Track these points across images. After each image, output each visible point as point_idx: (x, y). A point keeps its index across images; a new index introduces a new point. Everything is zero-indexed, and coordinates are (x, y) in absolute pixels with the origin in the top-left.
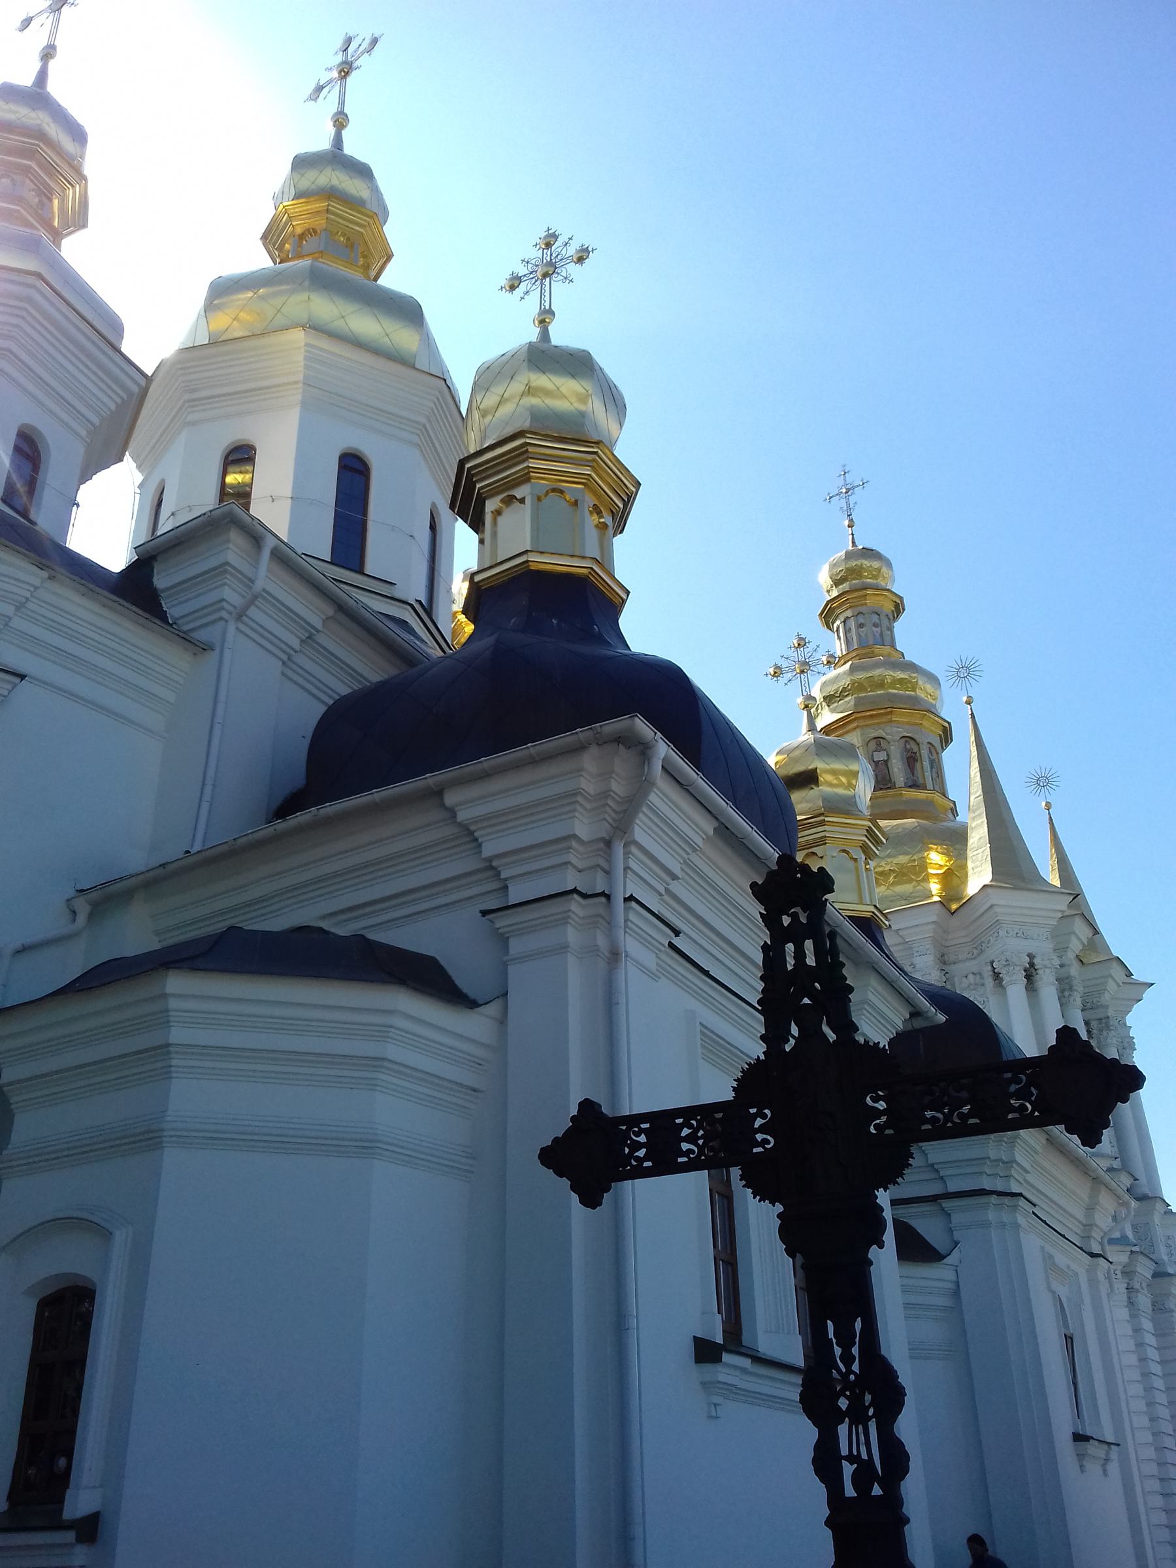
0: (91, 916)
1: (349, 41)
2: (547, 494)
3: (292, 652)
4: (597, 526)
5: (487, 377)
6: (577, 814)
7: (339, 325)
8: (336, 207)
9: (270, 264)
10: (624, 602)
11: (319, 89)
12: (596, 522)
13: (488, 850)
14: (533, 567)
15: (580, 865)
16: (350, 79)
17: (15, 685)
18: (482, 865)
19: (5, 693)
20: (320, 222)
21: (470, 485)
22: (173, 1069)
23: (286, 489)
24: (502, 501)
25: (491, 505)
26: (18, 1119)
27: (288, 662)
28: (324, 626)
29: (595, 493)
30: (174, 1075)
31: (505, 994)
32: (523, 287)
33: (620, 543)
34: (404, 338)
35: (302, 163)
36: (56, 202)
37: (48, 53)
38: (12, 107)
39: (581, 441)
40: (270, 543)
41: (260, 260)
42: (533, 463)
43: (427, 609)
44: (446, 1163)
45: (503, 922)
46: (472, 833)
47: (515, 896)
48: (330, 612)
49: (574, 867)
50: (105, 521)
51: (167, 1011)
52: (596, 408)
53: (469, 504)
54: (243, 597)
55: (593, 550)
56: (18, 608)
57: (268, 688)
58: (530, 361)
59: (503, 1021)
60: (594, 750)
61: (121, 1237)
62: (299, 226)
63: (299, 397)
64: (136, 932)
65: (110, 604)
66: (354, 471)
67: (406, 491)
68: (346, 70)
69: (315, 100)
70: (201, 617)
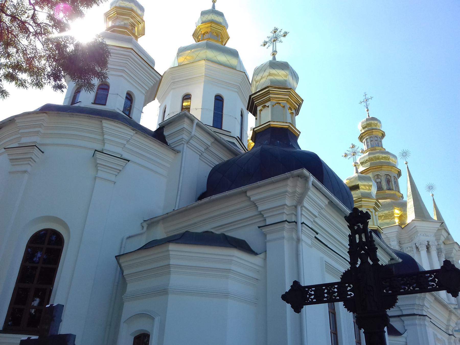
0: (147, 228)
5: (257, 72)
7: (215, 59)
8: (213, 25)
10: (299, 135)
13: (260, 208)
14: (272, 126)
20: (209, 30)
21: (253, 102)
25: (259, 108)
26: (128, 285)
31: (266, 251)
34: (233, 61)
35: (204, 13)
36: (136, 28)
38: (124, 2)
40: (196, 121)
41: (192, 41)
42: (271, 96)
43: (240, 139)
45: (265, 230)
46: (255, 204)
48: (213, 140)
50: (150, 117)
56: (127, 142)
57: (196, 163)
59: (265, 259)
60: (291, 179)
61: (157, 319)
63: (203, 80)
64: (160, 233)
66: (219, 100)
67: (234, 105)
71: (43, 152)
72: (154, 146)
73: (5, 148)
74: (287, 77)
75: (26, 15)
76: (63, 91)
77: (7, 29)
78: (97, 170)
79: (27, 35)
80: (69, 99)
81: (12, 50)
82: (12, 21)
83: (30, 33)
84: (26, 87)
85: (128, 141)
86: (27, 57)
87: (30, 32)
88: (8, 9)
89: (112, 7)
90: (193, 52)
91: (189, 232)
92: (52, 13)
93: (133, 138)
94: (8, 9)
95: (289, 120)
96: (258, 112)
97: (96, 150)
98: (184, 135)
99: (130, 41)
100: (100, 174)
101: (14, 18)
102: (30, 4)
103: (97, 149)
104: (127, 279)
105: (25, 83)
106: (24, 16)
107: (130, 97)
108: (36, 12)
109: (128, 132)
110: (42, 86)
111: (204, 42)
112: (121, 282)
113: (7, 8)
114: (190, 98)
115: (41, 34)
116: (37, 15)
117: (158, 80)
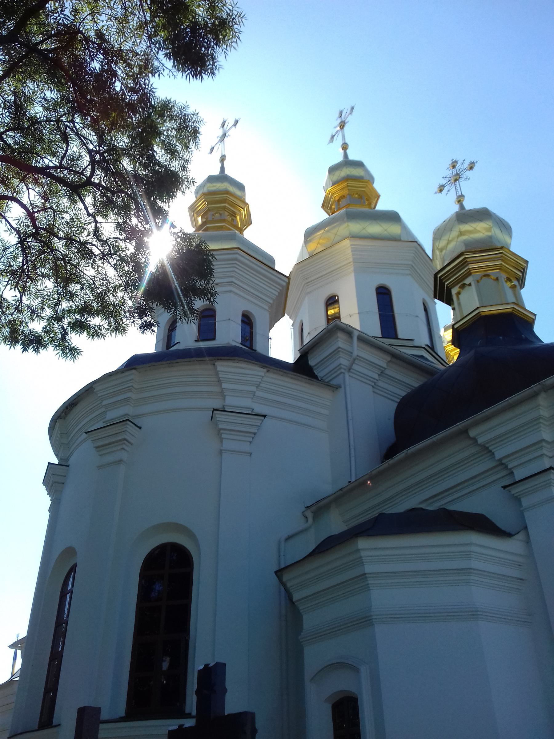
0: (314, 518)
1: (341, 113)
2: (481, 278)
3: (375, 381)
4: (511, 287)
5: (438, 234)
6: (542, 429)
7: (364, 232)
8: (351, 183)
9: (327, 216)
10: (534, 320)
11: (333, 137)
12: (510, 285)
13: (499, 454)
14: (483, 314)
15: (550, 454)
16: (346, 128)
17: (263, 420)
18: (498, 463)
19: (259, 424)
20: (345, 192)
21: (442, 284)
22: (370, 585)
23: (354, 309)
24: (460, 287)
25: (454, 291)
26: (305, 617)
27: (375, 386)
28: (387, 366)
29: (506, 272)
30: (371, 588)
31: (526, 528)
32: (446, 189)
33: (524, 292)
34: (394, 229)
35: (332, 170)
36: (238, 217)
37: (223, 159)
38: (214, 184)
39: (494, 250)
40: (356, 334)
41: (323, 216)
42: (471, 266)
43: (432, 348)
44: (516, 619)
45: (515, 490)
46: (487, 448)
47: (518, 477)
48: (389, 358)
49: (547, 456)
50: (282, 343)
51: (361, 557)
52: (497, 233)
53: (443, 293)
54: (349, 361)
55: (512, 299)
56: (257, 387)
57: (369, 399)
58: (458, 220)
59: (528, 541)
60: (543, 395)
61: (364, 671)
62: (337, 196)
63: (352, 269)
64: (336, 523)
65: (293, 376)
66: (384, 295)
67: (409, 297)
68: (342, 125)
69: (332, 142)
70: (330, 376)
71: (140, 428)
72: (298, 386)
73: (86, 433)
74: (491, 231)
75: (86, 233)
76: (153, 331)
77: (64, 259)
78: (221, 440)
79: (91, 261)
80: (161, 342)
81: (74, 287)
82: (67, 246)
83: (95, 257)
84: (103, 335)
85: (258, 386)
86: (97, 293)
87: (96, 256)
88: (60, 230)
89: (199, 196)
90: (328, 231)
91: (384, 513)
92: (121, 221)
93: (265, 379)
94: (60, 230)
95: (511, 298)
96: (455, 297)
97: (214, 410)
98: (341, 359)
99: (233, 237)
100: (227, 445)
101: (69, 240)
102: (89, 215)
103: (215, 407)
104: (300, 608)
105: (101, 330)
106: (83, 234)
107: (247, 320)
108: (98, 224)
109: (255, 372)
110: (124, 330)
111: (344, 210)
112: (291, 613)
113: (58, 229)
114: (337, 302)
115: (110, 255)
116: (101, 229)
117: (284, 284)
